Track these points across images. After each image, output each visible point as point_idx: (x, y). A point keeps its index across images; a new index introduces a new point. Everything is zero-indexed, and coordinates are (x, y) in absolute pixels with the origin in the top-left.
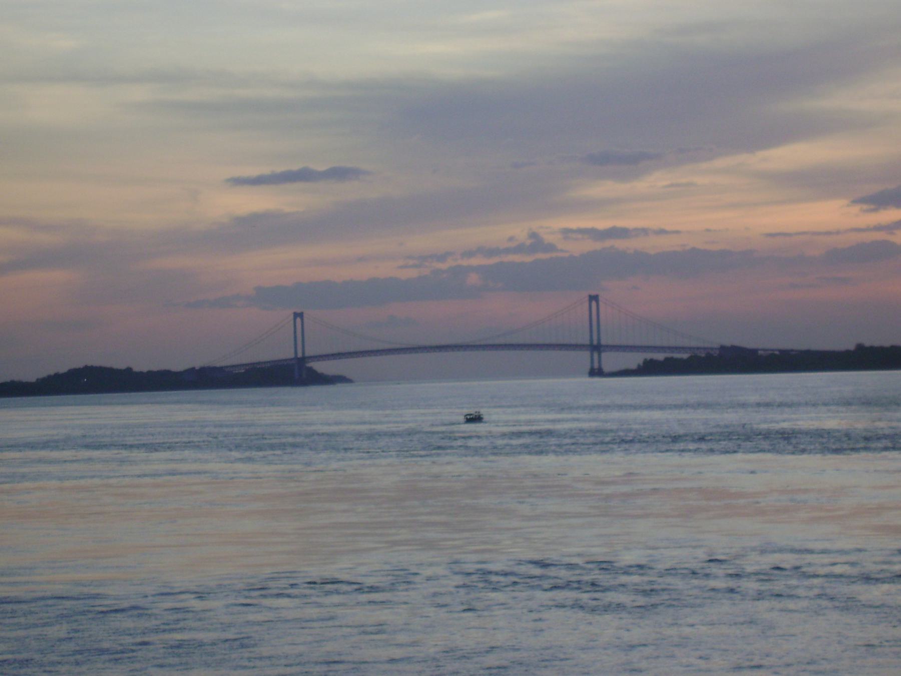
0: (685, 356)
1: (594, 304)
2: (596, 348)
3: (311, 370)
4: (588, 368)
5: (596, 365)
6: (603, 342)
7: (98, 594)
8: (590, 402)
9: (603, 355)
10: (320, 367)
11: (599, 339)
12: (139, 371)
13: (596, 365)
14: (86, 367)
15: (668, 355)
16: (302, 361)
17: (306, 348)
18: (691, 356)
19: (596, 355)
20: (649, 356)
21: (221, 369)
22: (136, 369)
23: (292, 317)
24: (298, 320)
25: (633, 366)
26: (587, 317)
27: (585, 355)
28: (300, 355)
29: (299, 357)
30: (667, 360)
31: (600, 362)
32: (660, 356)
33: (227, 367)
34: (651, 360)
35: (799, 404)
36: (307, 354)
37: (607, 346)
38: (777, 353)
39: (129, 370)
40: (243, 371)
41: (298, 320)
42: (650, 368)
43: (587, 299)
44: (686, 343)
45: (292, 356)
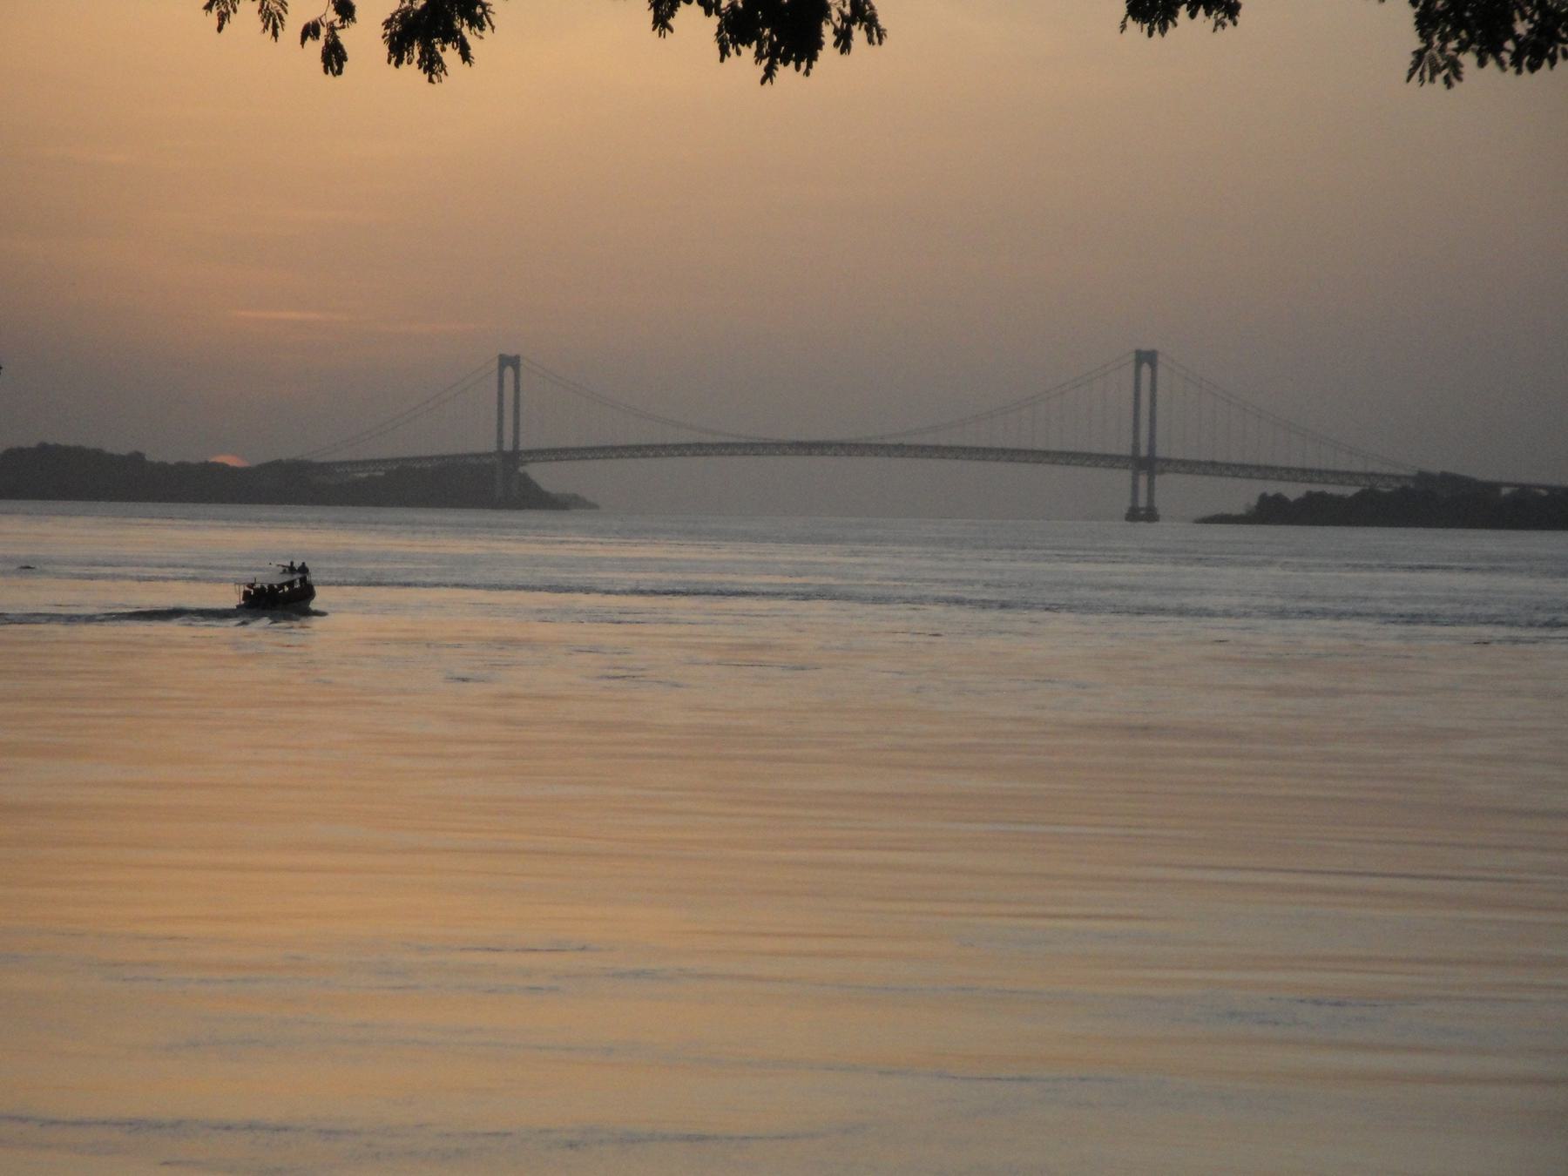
0: (1350, 491)
1: (1146, 369)
2: (1146, 464)
3: (526, 482)
4: (1126, 504)
5: (1142, 502)
6: (1161, 451)
7: (1408, 623)
8: (734, 663)
9: (1159, 480)
10: (543, 475)
11: (1152, 447)
12: (178, 459)
13: (1142, 502)
14: (43, 448)
15: (1316, 488)
16: (513, 458)
17: (522, 436)
18: (1363, 490)
19: (1143, 480)
20: (1272, 488)
21: (325, 468)
22: (154, 455)
23: (495, 365)
24: (1146, 370)
25: (1238, 509)
26: (1129, 393)
27: (1123, 478)
28: (508, 446)
29: (505, 449)
30: (1310, 497)
31: (1135, 488)
32: (1293, 491)
33: (341, 464)
34: (1322, 495)
35: (541, 950)
36: (523, 446)
37: (1169, 461)
38: (1544, 492)
39: (137, 458)
40: (382, 474)
41: (1146, 370)
42: (1271, 511)
43: (1132, 357)
44: (1358, 466)
45: (492, 447)
